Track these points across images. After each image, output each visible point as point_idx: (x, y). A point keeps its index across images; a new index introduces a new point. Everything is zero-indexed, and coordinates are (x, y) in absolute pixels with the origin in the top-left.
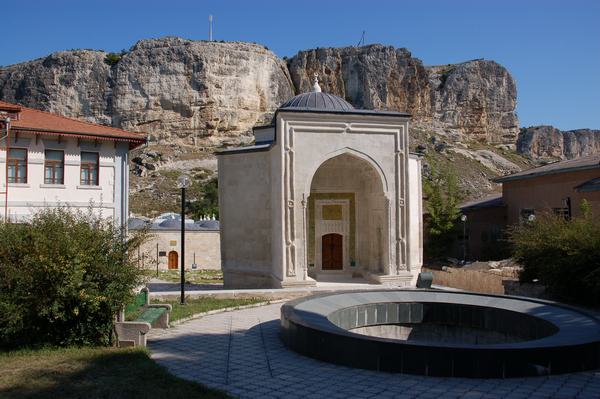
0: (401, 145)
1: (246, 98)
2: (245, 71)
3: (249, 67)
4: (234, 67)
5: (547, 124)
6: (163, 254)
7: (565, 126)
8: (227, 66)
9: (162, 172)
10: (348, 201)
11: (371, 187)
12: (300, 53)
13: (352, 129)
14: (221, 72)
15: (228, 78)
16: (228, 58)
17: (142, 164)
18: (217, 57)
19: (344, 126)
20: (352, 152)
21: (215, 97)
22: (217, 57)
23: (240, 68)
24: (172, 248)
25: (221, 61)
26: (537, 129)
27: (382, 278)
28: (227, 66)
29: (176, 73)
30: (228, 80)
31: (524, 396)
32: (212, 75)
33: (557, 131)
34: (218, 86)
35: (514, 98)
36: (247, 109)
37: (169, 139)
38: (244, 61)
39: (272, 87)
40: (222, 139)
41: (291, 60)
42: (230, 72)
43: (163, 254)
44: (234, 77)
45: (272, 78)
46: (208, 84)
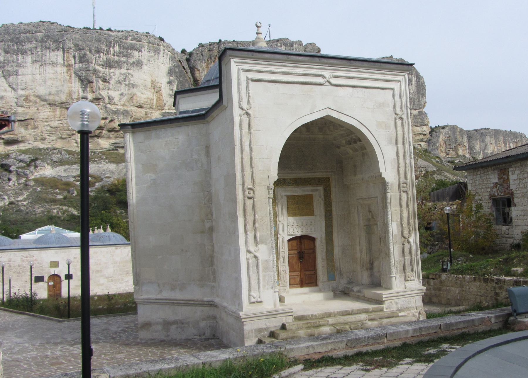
0: (401, 108)
1: (139, 94)
2: (139, 64)
3: (142, 59)
4: (124, 59)
5: (451, 123)
6: (39, 279)
7: (469, 125)
8: (116, 58)
9: (36, 180)
10: (321, 188)
11: (355, 166)
12: (201, 45)
13: (334, 81)
14: (109, 64)
15: (117, 71)
16: (117, 49)
17: (10, 172)
18: (104, 47)
19: (323, 76)
20: (335, 115)
21: (104, 93)
22: (104, 47)
23: (131, 61)
24: (53, 271)
25: (108, 52)
26: (443, 128)
27: (384, 294)
28: (116, 58)
29: (54, 64)
30: (116, 74)
31: (359, 376)
32: (97, 67)
33: (461, 130)
34: (105, 80)
35: (424, 95)
36: (140, 107)
37: (46, 141)
38: (136, 53)
39: (170, 83)
40: (112, 141)
41: (191, 54)
42: (119, 65)
43: (39, 279)
44: (124, 71)
45: (171, 72)
46: (94, 78)
